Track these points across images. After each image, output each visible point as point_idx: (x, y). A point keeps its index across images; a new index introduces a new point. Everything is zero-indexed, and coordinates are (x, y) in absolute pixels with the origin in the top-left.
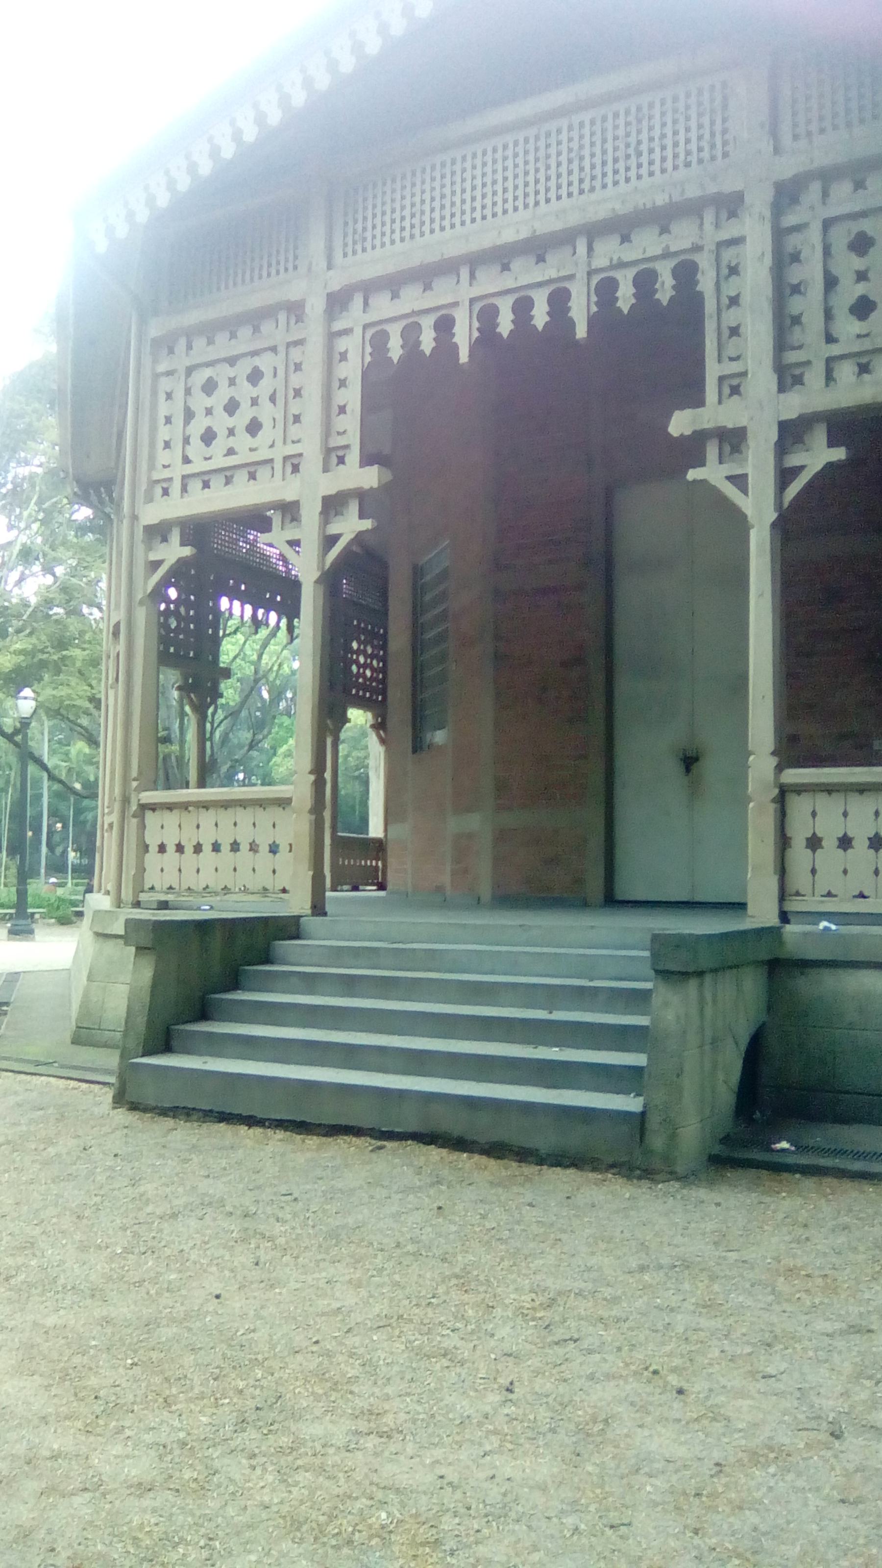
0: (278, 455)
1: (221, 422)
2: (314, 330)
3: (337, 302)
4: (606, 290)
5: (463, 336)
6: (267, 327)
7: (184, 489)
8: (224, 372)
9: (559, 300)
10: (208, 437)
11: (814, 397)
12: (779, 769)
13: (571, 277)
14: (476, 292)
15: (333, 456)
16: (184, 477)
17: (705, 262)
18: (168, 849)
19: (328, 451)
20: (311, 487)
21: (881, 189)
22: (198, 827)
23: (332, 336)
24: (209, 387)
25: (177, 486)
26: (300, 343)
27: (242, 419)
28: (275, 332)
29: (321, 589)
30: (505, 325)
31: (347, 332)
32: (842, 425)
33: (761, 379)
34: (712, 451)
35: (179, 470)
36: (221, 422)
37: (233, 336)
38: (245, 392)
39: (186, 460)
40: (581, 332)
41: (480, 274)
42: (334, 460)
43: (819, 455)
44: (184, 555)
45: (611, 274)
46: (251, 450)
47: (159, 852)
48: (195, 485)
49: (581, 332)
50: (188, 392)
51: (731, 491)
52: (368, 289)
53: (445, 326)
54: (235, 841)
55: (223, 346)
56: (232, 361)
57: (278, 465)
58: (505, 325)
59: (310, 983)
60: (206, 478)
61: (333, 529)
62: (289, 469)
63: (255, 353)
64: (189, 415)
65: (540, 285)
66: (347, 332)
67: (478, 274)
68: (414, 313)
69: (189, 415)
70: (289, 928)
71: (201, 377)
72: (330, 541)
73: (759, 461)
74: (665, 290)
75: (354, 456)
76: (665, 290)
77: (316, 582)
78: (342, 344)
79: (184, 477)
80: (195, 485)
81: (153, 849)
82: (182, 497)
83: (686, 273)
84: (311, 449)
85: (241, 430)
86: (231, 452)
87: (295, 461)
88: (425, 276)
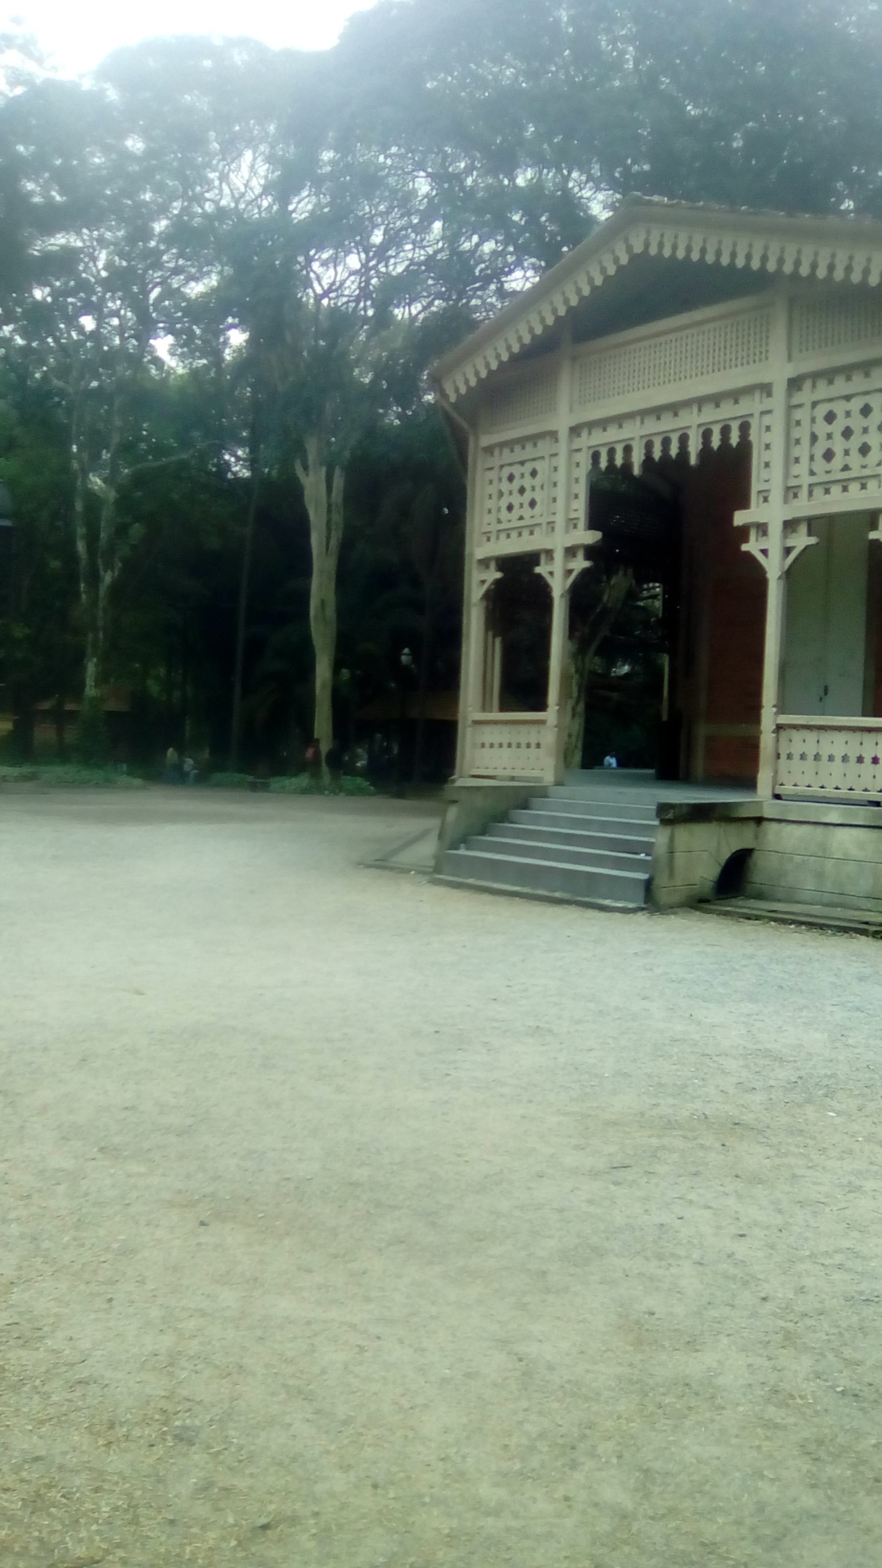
0: (543, 520)
1: (838, 445)
2: (563, 447)
3: (575, 431)
4: (707, 435)
5: (694, 447)
6: (540, 444)
7: (810, 493)
8: (839, 408)
9: (684, 440)
10: (829, 455)
11: (804, 507)
12: (777, 714)
13: (751, 415)
14: (702, 421)
15: (572, 523)
16: (810, 485)
17: (754, 423)
18: (865, 760)
19: (788, 489)
20: (559, 541)
21: (881, 378)
22: (877, 744)
23: (791, 408)
24: (830, 418)
25: (804, 492)
26: (769, 412)
27: (855, 442)
28: (544, 447)
29: (782, 582)
30: (716, 442)
31: (800, 406)
32: (812, 523)
33: (776, 495)
34: (543, 559)
35: (806, 480)
36: (516, 499)
37: (512, 451)
38: (857, 422)
39: (812, 473)
40: (693, 460)
41: (704, 409)
42: (791, 495)
43: (802, 540)
44: (810, 543)
45: (667, 435)
46: (828, 472)
47: (815, 760)
48: (818, 492)
49: (693, 460)
50: (813, 420)
51: (760, 557)
52: (591, 425)
53: (628, 450)
54: (818, 753)
55: (841, 386)
56: (522, 463)
57: (544, 526)
58: (716, 442)
59: (555, 821)
60: (827, 486)
61: (790, 543)
62: (762, 499)
63: (831, 400)
64: (814, 438)
65: (658, 434)
66: (800, 406)
67: (645, 421)
68: (651, 435)
69: (501, 494)
70: (541, 792)
71: (506, 472)
72: (788, 551)
73: (774, 542)
74: (734, 439)
75: (582, 523)
76: (734, 439)
77: (780, 578)
78: (798, 415)
79: (810, 485)
80: (818, 492)
81: (783, 756)
82: (809, 500)
83: (745, 428)
84: (560, 520)
85: (526, 505)
86: (521, 518)
87: (766, 494)
88: (674, 408)
